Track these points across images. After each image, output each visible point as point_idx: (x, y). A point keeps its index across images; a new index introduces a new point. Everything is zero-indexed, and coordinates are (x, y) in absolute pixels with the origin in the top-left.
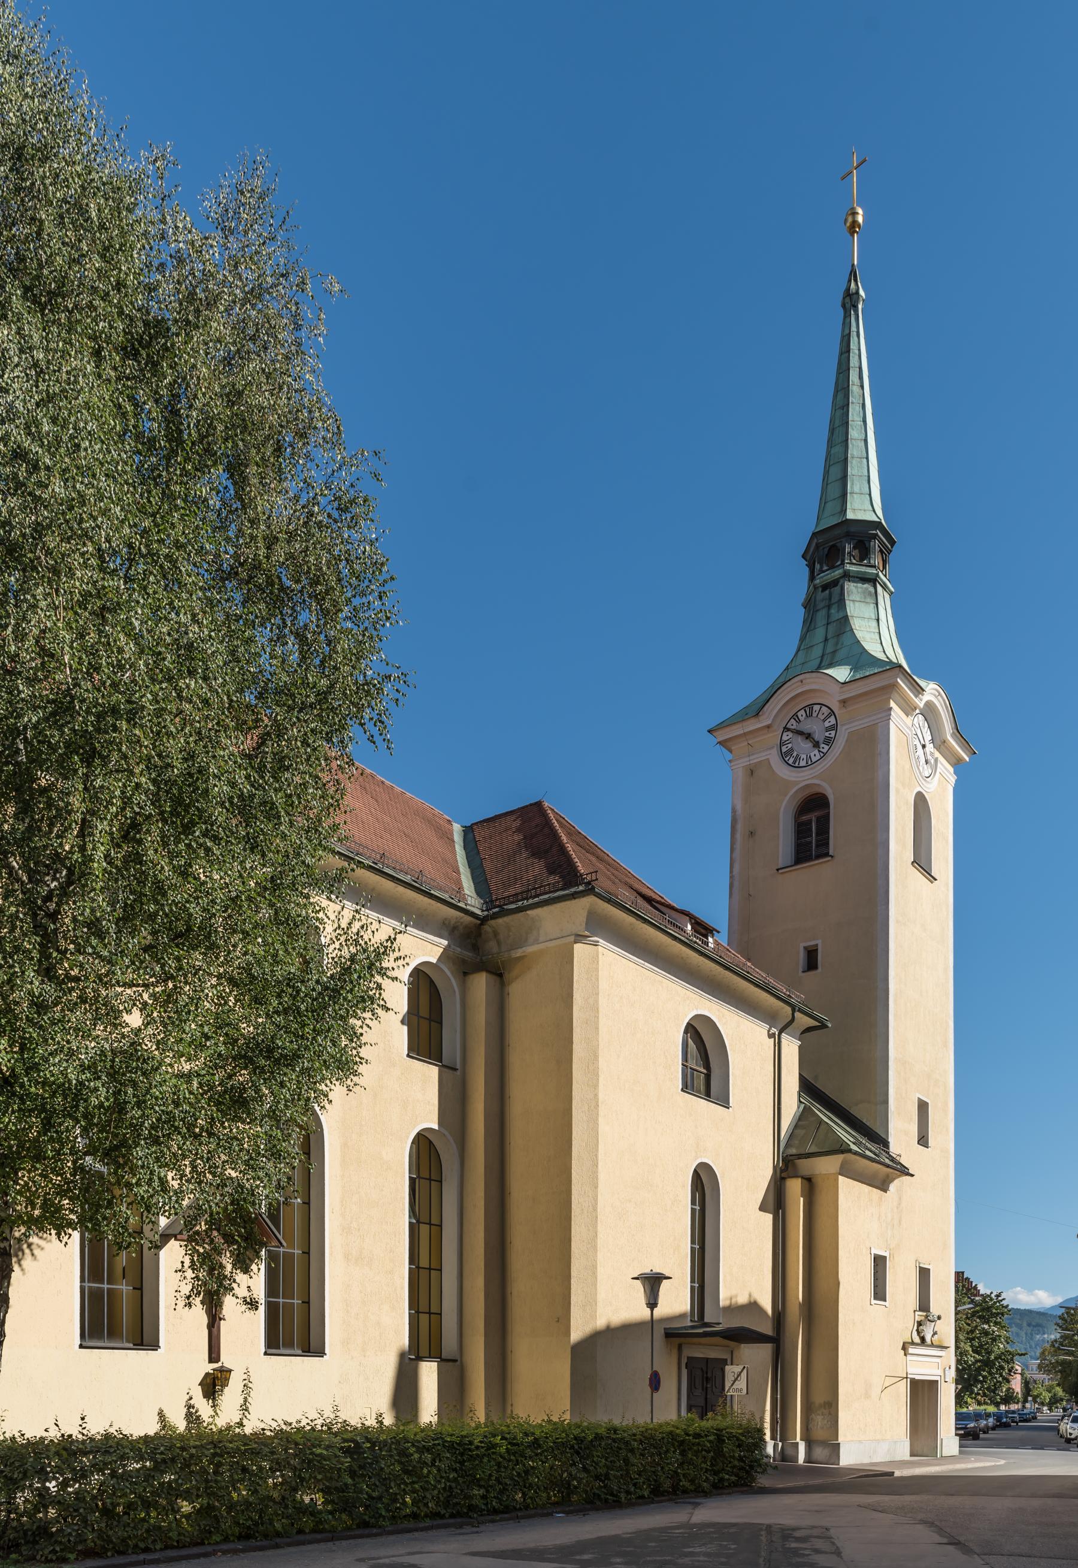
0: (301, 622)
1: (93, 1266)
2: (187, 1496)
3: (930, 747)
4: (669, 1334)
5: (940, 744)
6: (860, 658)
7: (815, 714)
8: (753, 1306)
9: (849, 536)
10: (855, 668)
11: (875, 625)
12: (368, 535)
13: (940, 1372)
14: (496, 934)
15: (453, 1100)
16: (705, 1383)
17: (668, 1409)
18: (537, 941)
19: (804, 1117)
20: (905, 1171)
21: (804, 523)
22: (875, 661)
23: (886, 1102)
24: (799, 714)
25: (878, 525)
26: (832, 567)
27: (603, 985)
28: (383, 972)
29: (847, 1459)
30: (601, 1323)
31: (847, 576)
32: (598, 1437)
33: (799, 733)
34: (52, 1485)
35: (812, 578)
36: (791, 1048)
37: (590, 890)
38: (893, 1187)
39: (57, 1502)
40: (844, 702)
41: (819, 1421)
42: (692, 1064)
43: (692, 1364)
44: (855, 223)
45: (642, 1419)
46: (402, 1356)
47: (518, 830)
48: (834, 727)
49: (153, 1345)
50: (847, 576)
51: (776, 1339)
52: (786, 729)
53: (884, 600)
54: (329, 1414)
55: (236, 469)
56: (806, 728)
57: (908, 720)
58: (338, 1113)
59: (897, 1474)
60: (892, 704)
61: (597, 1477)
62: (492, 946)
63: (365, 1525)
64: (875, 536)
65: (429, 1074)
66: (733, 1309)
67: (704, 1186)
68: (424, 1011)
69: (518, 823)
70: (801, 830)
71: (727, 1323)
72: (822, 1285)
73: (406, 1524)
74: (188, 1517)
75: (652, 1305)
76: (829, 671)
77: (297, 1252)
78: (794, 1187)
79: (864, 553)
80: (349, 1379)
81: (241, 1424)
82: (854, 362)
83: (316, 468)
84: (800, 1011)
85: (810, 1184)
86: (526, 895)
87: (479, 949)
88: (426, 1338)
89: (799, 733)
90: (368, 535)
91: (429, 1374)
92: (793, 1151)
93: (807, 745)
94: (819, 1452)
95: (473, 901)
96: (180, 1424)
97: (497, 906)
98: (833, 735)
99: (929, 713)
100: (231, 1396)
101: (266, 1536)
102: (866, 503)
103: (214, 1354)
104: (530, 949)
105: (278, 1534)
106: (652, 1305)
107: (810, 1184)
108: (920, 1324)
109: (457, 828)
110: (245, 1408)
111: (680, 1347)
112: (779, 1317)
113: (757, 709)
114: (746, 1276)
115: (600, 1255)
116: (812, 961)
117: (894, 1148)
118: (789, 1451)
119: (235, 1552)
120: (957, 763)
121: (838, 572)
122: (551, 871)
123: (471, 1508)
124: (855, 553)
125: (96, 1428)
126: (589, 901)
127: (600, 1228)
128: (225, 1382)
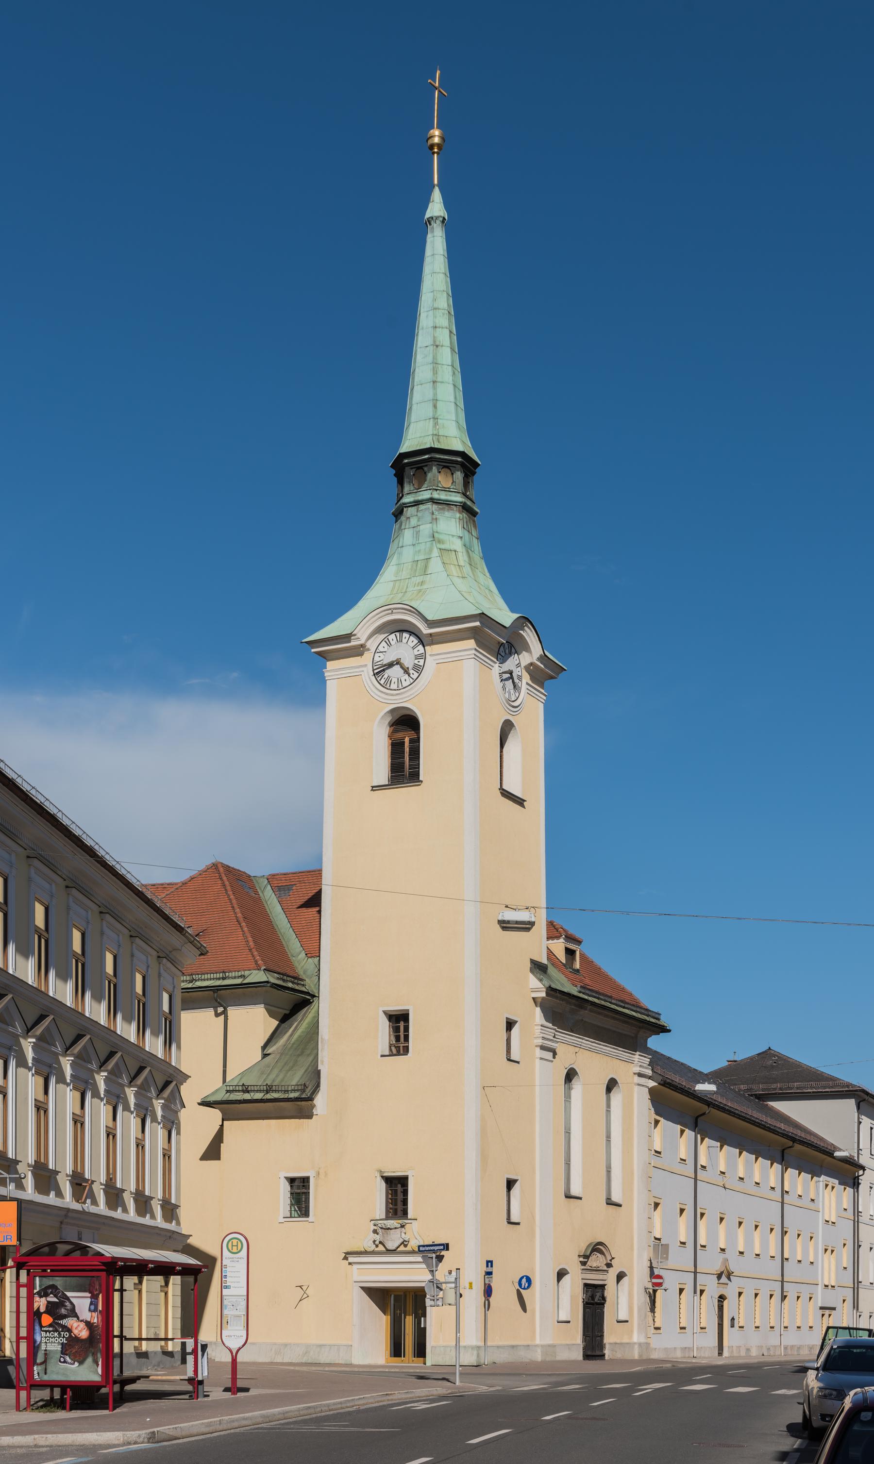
7: (404, 641)
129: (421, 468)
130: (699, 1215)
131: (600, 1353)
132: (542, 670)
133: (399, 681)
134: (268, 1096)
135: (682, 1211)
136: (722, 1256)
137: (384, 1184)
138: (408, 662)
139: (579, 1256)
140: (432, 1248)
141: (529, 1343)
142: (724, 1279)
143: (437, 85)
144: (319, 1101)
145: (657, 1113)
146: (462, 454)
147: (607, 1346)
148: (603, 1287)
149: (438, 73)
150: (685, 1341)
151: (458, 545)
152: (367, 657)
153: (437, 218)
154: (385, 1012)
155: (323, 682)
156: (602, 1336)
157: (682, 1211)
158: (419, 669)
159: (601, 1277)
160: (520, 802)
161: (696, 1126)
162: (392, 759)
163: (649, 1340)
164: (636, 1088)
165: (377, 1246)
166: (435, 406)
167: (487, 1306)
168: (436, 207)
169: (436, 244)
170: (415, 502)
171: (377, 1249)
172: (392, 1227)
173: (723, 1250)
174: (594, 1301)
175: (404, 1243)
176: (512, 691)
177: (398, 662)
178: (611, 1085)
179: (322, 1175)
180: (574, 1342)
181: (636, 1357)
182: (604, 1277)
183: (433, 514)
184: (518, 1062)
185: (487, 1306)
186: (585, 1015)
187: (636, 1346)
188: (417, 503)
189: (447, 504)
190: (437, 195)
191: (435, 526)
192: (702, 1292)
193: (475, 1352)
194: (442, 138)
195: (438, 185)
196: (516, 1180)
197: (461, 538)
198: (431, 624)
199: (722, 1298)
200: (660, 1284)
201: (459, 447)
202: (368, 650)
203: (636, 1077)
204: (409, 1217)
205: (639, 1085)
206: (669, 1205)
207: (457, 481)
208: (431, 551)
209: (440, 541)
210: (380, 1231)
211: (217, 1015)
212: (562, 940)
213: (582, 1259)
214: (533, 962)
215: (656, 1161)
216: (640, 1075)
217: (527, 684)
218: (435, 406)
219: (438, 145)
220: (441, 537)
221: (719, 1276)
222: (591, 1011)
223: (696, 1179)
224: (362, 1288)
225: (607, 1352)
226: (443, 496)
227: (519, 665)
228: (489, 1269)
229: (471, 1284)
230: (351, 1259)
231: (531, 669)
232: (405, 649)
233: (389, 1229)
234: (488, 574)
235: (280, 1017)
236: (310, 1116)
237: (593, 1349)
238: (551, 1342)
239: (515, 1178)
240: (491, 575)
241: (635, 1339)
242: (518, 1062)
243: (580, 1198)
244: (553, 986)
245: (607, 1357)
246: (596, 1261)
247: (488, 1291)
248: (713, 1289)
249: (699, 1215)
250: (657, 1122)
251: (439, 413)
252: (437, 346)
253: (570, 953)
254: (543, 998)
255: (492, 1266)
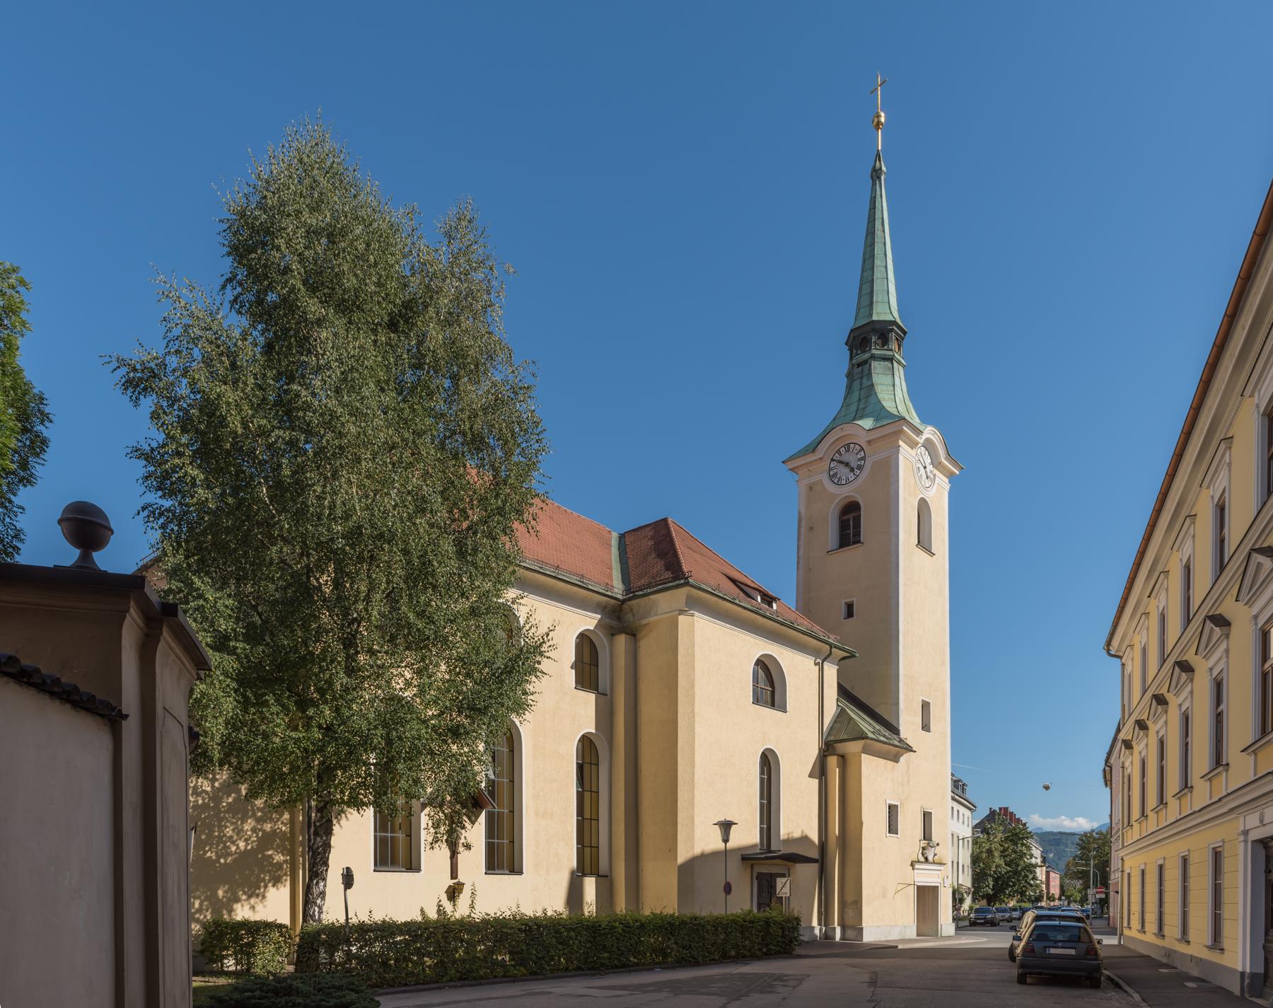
0: (485, 471)
1: (382, 824)
2: (429, 955)
3: (930, 468)
4: (745, 858)
5: (937, 464)
6: (881, 414)
8: (805, 839)
9: (874, 331)
10: (877, 420)
11: (893, 389)
12: (524, 407)
13: (940, 880)
14: (631, 610)
15: (605, 715)
16: (766, 886)
17: (742, 902)
18: (656, 614)
19: (841, 715)
20: (909, 749)
21: (847, 322)
22: (890, 415)
23: (898, 704)
25: (894, 323)
26: (864, 352)
27: (698, 640)
28: (541, 654)
29: (869, 936)
30: (697, 851)
31: (873, 357)
32: (683, 923)
33: (841, 462)
34: (354, 949)
35: (851, 358)
36: (831, 671)
37: (687, 584)
38: (902, 759)
39: (357, 957)
40: (869, 442)
41: (850, 913)
42: (761, 685)
43: (760, 877)
44: (879, 123)
45: (718, 911)
46: (573, 873)
47: (652, 538)
48: (863, 459)
49: (418, 869)
50: (873, 357)
51: (822, 861)
52: (833, 460)
53: (899, 372)
54: (514, 909)
55: (455, 378)
56: (846, 461)
57: (913, 452)
58: (528, 727)
59: (900, 947)
60: (901, 443)
61: (684, 948)
62: (629, 617)
63: (535, 973)
64: (892, 330)
65: (588, 700)
66: (790, 841)
67: (768, 762)
68: (587, 659)
69: (651, 534)
70: (843, 525)
71: (785, 850)
72: (851, 825)
73: (560, 974)
74: (429, 967)
75: (726, 841)
76: (859, 422)
77: (506, 811)
78: (833, 761)
79: (885, 341)
80: (540, 887)
81: (469, 916)
82: (878, 215)
83: (498, 374)
84: (836, 647)
85: (843, 758)
86: (649, 586)
87: (620, 619)
88: (588, 862)
89: (841, 462)
90: (524, 407)
91: (590, 885)
92: (832, 738)
93: (847, 470)
94: (850, 933)
95: (618, 589)
96: (433, 915)
97: (632, 591)
99: (928, 445)
100: (464, 899)
101: (475, 979)
102: (888, 307)
103: (454, 874)
104: (652, 619)
105: (482, 978)
106: (726, 841)
107: (843, 758)
108: (924, 849)
109: (615, 535)
110: (472, 906)
111: (752, 866)
112: (823, 846)
113: (813, 447)
114: (799, 818)
115: (696, 810)
116: (850, 612)
117: (902, 736)
118: (830, 933)
119: (456, 987)
120: (950, 476)
121: (867, 355)
122: (667, 569)
123: (602, 965)
124: (879, 342)
125: (378, 917)
126: (685, 591)
127: (696, 793)
128: (461, 891)
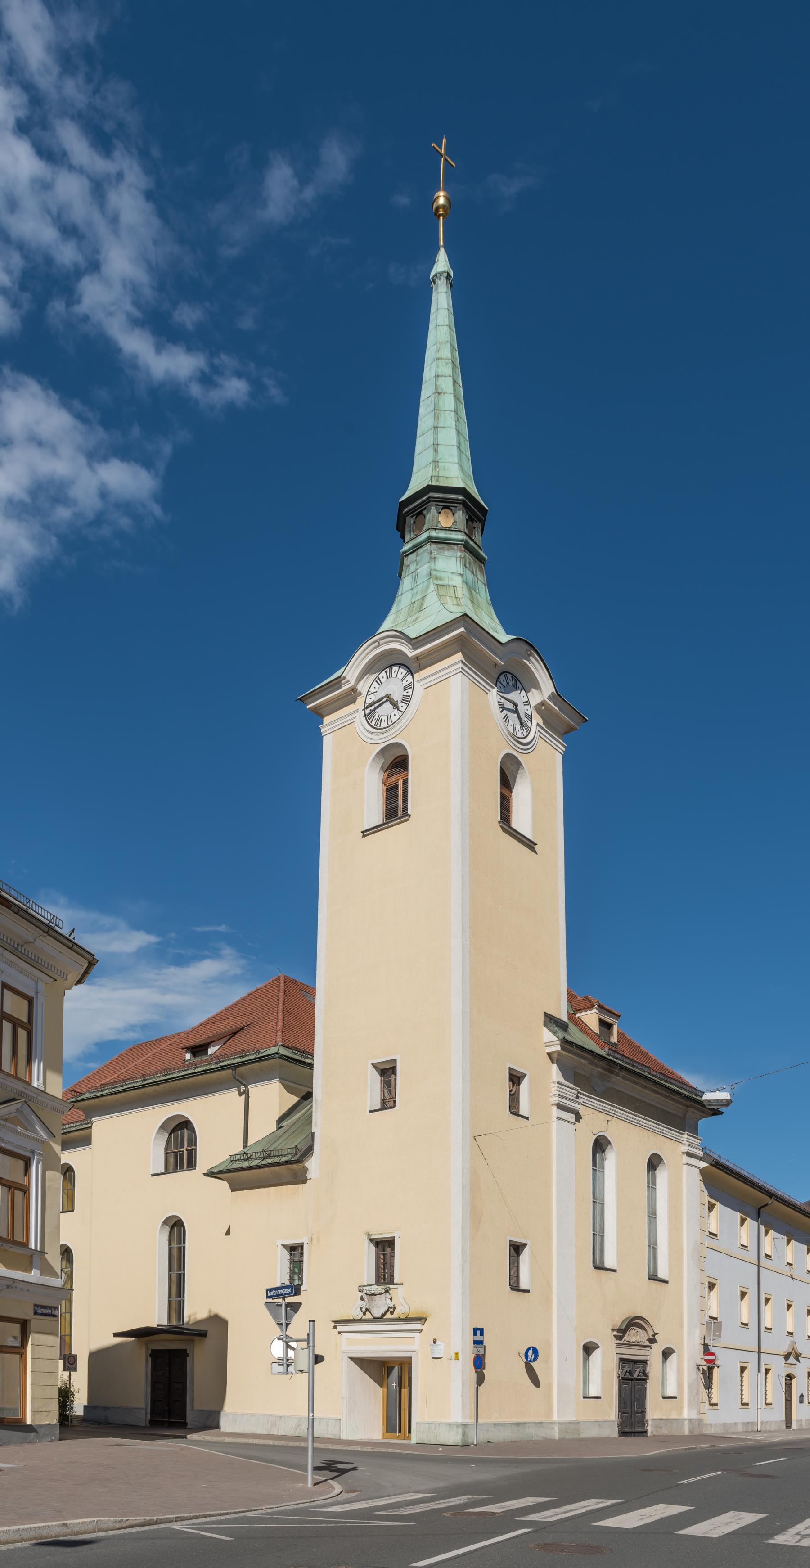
7: (394, 675)
24: (380, 676)
98: (410, 694)
129: (421, 513)
130: (763, 1301)
131: (642, 1430)
132: (557, 715)
133: (389, 717)
134: (264, 1162)
135: (743, 1295)
136: (790, 1338)
137: (373, 1248)
138: (397, 697)
139: (613, 1330)
140: (279, 1292)
141: (543, 1420)
142: (792, 1360)
143: (443, 152)
144: (313, 1165)
145: (711, 1196)
146: (463, 491)
147: (650, 1423)
148: (645, 1362)
149: (444, 141)
150: (748, 1416)
151: (458, 581)
152: (360, 704)
153: (441, 273)
154: (374, 1065)
155: (319, 739)
156: (643, 1412)
157: (743, 1295)
158: (406, 700)
159: (642, 1352)
160: (531, 845)
161: (759, 1216)
162: (387, 804)
163: (702, 1416)
164: (685, 1167)
165: (364, 1314)
166: (436, 450)
167: (480, 1380)
168: (442, 264)
169: (441, 301)
170: (414, 547)
171: (364, 1317)
172: (376, 1292)
173: (791, 1334)
174: (633, 1380)
175: (391, 1310)
176: (518, 727)
177: (388, 698)
178: (654, 1163)
179: (315, 1242)
180: (606, 1418)
181: (687, 1433)
182: (647, 1353)
183: (431, 553)
184: (527, 1118)
185: (480, 1380)
186: (619, 1082)
187: (686, 1422)
188: (417, 548)
189: (447, 543)
190: (442, 255)
191: (433, 564)
192: (767, 1371)
193: (460, 1431)
194: (447, 198)
195: (445, 246)
196: (525, 1245)
197: (462, 575)
198: (415, 642)
199: (790, 1377)
200: (713, 1361)
201: (460, 484)
202: (360, 694)
203: (685, 1156)
204: (395, 1282)
205: (687, 1164)
206: (728, 1286)
207: (458, 521)
208: (427, 588)
209: (437, 578)
210: (365, 1297)
211: (240, 1094)
212: (595, 1010)
213: (615, 1333)
214: (546, 1015)
215: (709, 1242)
216: (689, 1154)
217: (538, 725)
218: (436, 450)
219: (444, 207)
220: (439, 574)
221: (787, 1357)
222: (624, 1078)
223: (759, 1266)
224: (351, 1358)
225: (650, 1429)
226: (442, 534)
227: (527, 703)
228: (478, 1338)
229: (457, 1354)
230: (340, 1328)
231: (541, 708)
232: (394, 683)
233: (373, 1294)
234: (497, 621)
235: (302, 1095)
236: (304, 1181)
237: (632, 1425)
238: (573, 1419)
239: (524, 1241)
240: (501, 622)
241: (685, 1414)
242: (527, 1118)
243: (615, 1271)
244: (568, 1038)
245: (649, 1434)
246: (633, 1336)
247: (479, 1362)
248: (779, 1368)
249: (763, 1301)
250: (711, 1207)
251: (440, 456)
252: (439, 394)
253: (606, 1026)
254: (558, 1053)
255: (482, 1334)
